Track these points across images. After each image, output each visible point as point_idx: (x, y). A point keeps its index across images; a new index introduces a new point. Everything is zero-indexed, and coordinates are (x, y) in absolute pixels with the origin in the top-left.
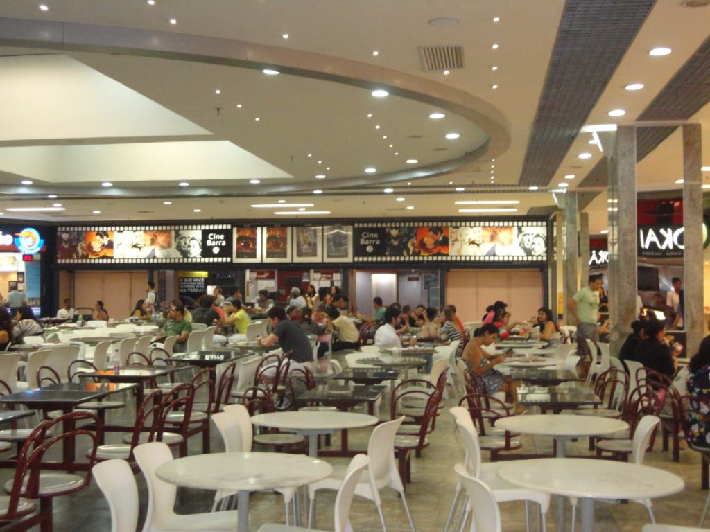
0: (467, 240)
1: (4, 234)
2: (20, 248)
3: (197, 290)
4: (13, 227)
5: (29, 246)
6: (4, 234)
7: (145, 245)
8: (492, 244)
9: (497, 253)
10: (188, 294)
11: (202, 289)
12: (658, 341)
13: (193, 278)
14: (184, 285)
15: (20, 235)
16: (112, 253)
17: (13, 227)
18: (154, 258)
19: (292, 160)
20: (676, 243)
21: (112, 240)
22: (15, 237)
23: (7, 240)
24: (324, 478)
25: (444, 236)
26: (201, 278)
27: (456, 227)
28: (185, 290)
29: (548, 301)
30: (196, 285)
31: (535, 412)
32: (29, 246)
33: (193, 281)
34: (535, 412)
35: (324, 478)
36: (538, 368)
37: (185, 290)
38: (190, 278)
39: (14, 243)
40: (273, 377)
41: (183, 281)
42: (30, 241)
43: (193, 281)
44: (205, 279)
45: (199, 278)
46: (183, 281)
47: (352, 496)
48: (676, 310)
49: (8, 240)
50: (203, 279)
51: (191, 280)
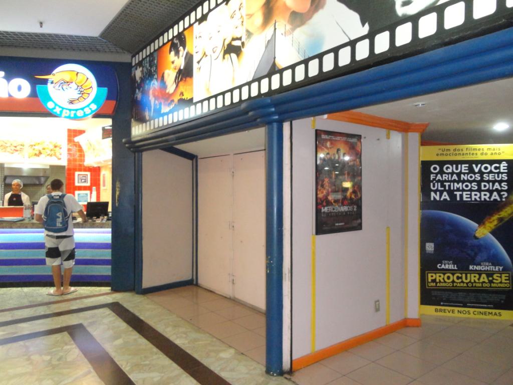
0: (338, 147)
1: (8, 77)
2: (50, 105)
3: (485, 196)
4: (30, 58)
5: (71, 102)
6: (8, 77)
7: (249, 34)
8: (270, 30)
9: (281, 63)
13: (470, 163)
14: (442, 183)
15: (50, 77)
16: (192, 91)
17: (30, 58)
18: (274, 70)
19: (41, 27)
20: (359, 143)
21: (190, 52)
22: (34, 82)
23: (20, 88)
24: (347, 36)
25: (187, 53)
26: (499, 162)
27: (204, 18)
28: (445, 196)
32: (71, 102)
33: (471, 170)
35: (347, 36)
37: (445, 196)
38: (457, 163)
39: (34, 94)
41: (442, 172)
42: (72, 92)
43: (471, 170)
45: (491, 162)
46: (442, 172)
49: (20, 88)
50: (503, 167)
51: (464, 168)
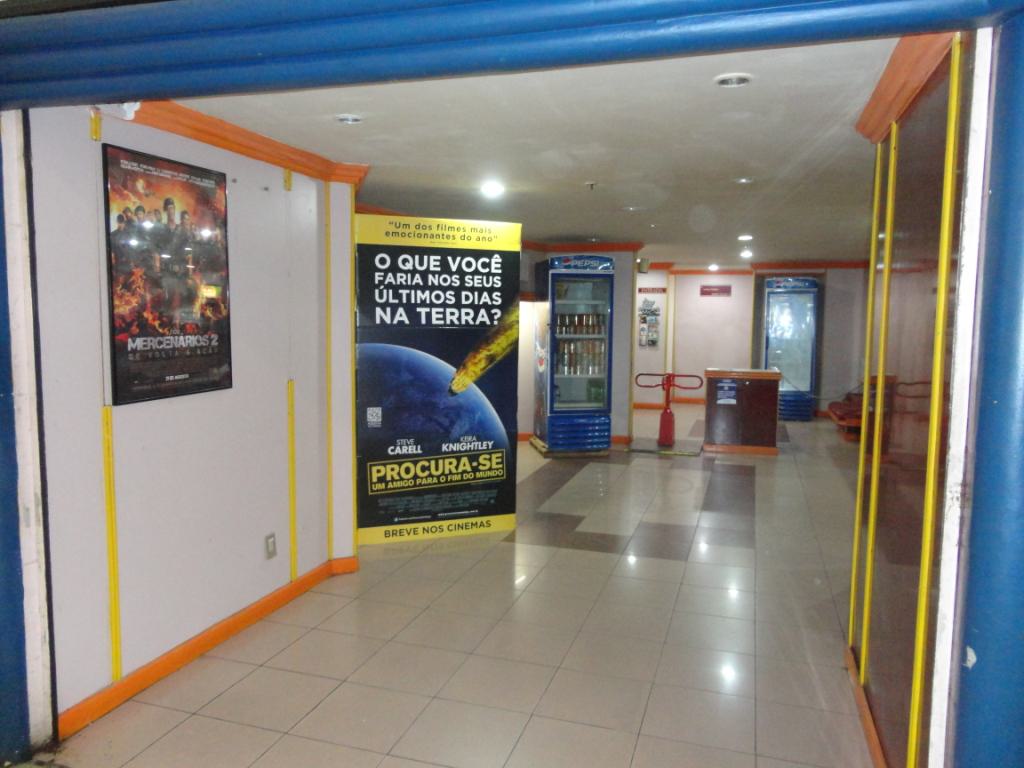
3: (467, 317)
10: (419, 334)
11: (488, 308)
12: (466, 355)
13: (444, 253)
14: (396, 288)
26: (489, 254)
28: (401, 316)
29: (864, 571)
30: (458, 291)
31: (897, 235)
33: (445, 268)
34: (897, 235)
36: (429, 517)
37: (401, 316)
40: (791, 306)
41: (394, 269)
43: (445, 268)
44: (509, 258)
45: (477, 254)
46: (394, 269)
47: (517, 510)
48: (1001, 13)
51: (433, 262)
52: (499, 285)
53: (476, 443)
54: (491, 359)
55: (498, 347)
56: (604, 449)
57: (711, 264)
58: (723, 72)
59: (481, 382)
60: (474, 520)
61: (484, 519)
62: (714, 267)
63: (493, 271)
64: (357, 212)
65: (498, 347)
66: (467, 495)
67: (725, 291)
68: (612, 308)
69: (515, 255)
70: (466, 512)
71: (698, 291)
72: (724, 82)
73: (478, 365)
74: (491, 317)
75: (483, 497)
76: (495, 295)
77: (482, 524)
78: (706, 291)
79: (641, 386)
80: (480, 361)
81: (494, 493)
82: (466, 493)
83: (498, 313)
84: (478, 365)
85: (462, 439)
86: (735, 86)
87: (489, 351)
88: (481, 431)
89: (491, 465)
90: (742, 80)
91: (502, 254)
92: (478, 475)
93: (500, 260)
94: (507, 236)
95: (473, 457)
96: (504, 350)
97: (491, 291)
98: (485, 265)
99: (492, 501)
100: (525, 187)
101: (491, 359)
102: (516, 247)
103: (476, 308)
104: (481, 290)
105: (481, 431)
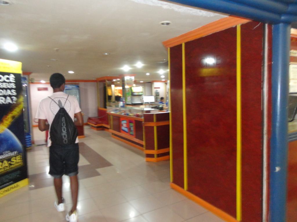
11: (10, 96)
26: (9, 74)
50: (12, 78)
52: (14, 87)
53: (9, 153)
54: (13, 117)
55: (16, 112)
56: (30, 147)
57: (147, 73)
58: (164, 21)
59: (10, 128)
60: (11, 186)
61: (15, 184)
62: (43, 82)
63: (12, 81)
64: (172, 49)
65: (16, 112)
66: (7, 176)
67: (46, 89)
68: (27, 95)
69: (19, 75)
70: (8, 184)
71: (36, 89)
72: (163, 24)
73: (8, 120)
74: (12, 99)
75: (14, 175)
76: (13, 91)
77: (15, 187)
78: (39, 89)
79: (36, 122)
80: (8, 118)
81: (19, 172)
82: (7, 176)
83: (15, 98)
84: (8, 120)
85: (3, 153)
86: (165, 25)
87: (12, 114)
88: (12, 148)
89: (17, 161)
90: (168, 24)
91: (15, 74)
92: (12, 166)
93: (14, 77)
94: (16, 67)
95: (9, 159)
96: (18, 113)
97: (10, 89)
98: (8, 79)
99: (18, 176)
100: (28, 48)
101: (13, 117)
102: (20, 72)
103: (5, 96)
104: (6, 89)
105: (12, 148)
